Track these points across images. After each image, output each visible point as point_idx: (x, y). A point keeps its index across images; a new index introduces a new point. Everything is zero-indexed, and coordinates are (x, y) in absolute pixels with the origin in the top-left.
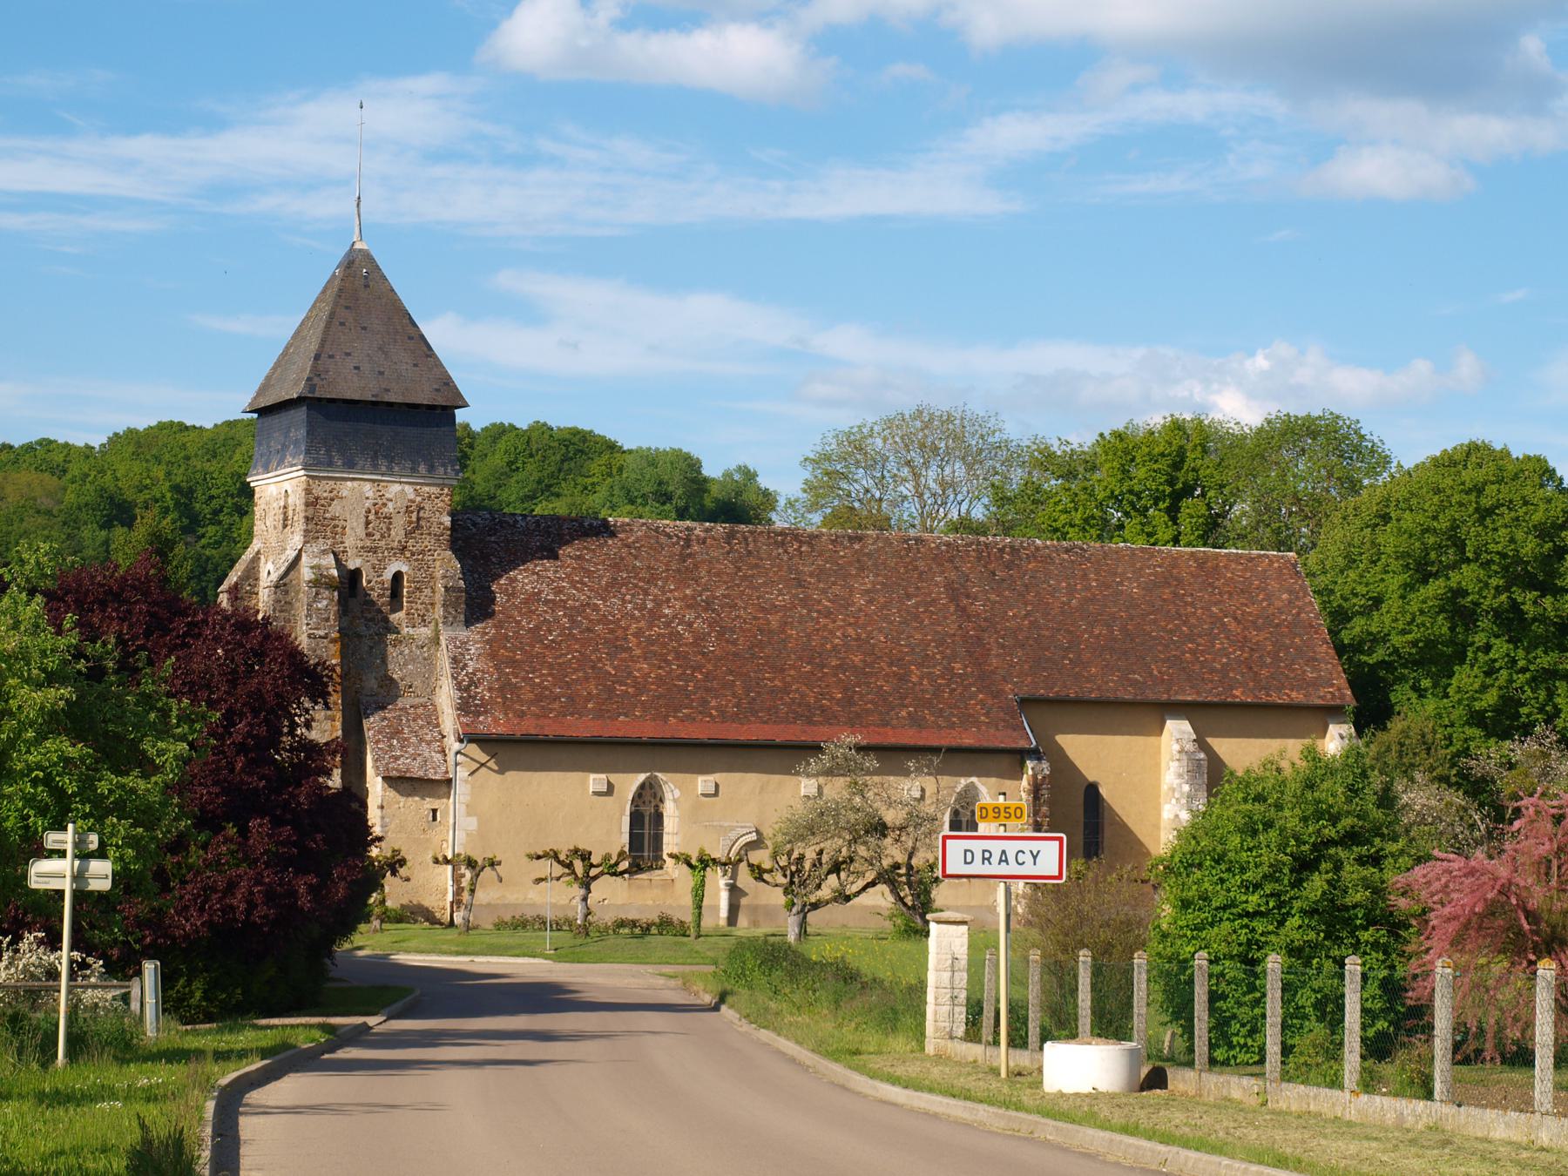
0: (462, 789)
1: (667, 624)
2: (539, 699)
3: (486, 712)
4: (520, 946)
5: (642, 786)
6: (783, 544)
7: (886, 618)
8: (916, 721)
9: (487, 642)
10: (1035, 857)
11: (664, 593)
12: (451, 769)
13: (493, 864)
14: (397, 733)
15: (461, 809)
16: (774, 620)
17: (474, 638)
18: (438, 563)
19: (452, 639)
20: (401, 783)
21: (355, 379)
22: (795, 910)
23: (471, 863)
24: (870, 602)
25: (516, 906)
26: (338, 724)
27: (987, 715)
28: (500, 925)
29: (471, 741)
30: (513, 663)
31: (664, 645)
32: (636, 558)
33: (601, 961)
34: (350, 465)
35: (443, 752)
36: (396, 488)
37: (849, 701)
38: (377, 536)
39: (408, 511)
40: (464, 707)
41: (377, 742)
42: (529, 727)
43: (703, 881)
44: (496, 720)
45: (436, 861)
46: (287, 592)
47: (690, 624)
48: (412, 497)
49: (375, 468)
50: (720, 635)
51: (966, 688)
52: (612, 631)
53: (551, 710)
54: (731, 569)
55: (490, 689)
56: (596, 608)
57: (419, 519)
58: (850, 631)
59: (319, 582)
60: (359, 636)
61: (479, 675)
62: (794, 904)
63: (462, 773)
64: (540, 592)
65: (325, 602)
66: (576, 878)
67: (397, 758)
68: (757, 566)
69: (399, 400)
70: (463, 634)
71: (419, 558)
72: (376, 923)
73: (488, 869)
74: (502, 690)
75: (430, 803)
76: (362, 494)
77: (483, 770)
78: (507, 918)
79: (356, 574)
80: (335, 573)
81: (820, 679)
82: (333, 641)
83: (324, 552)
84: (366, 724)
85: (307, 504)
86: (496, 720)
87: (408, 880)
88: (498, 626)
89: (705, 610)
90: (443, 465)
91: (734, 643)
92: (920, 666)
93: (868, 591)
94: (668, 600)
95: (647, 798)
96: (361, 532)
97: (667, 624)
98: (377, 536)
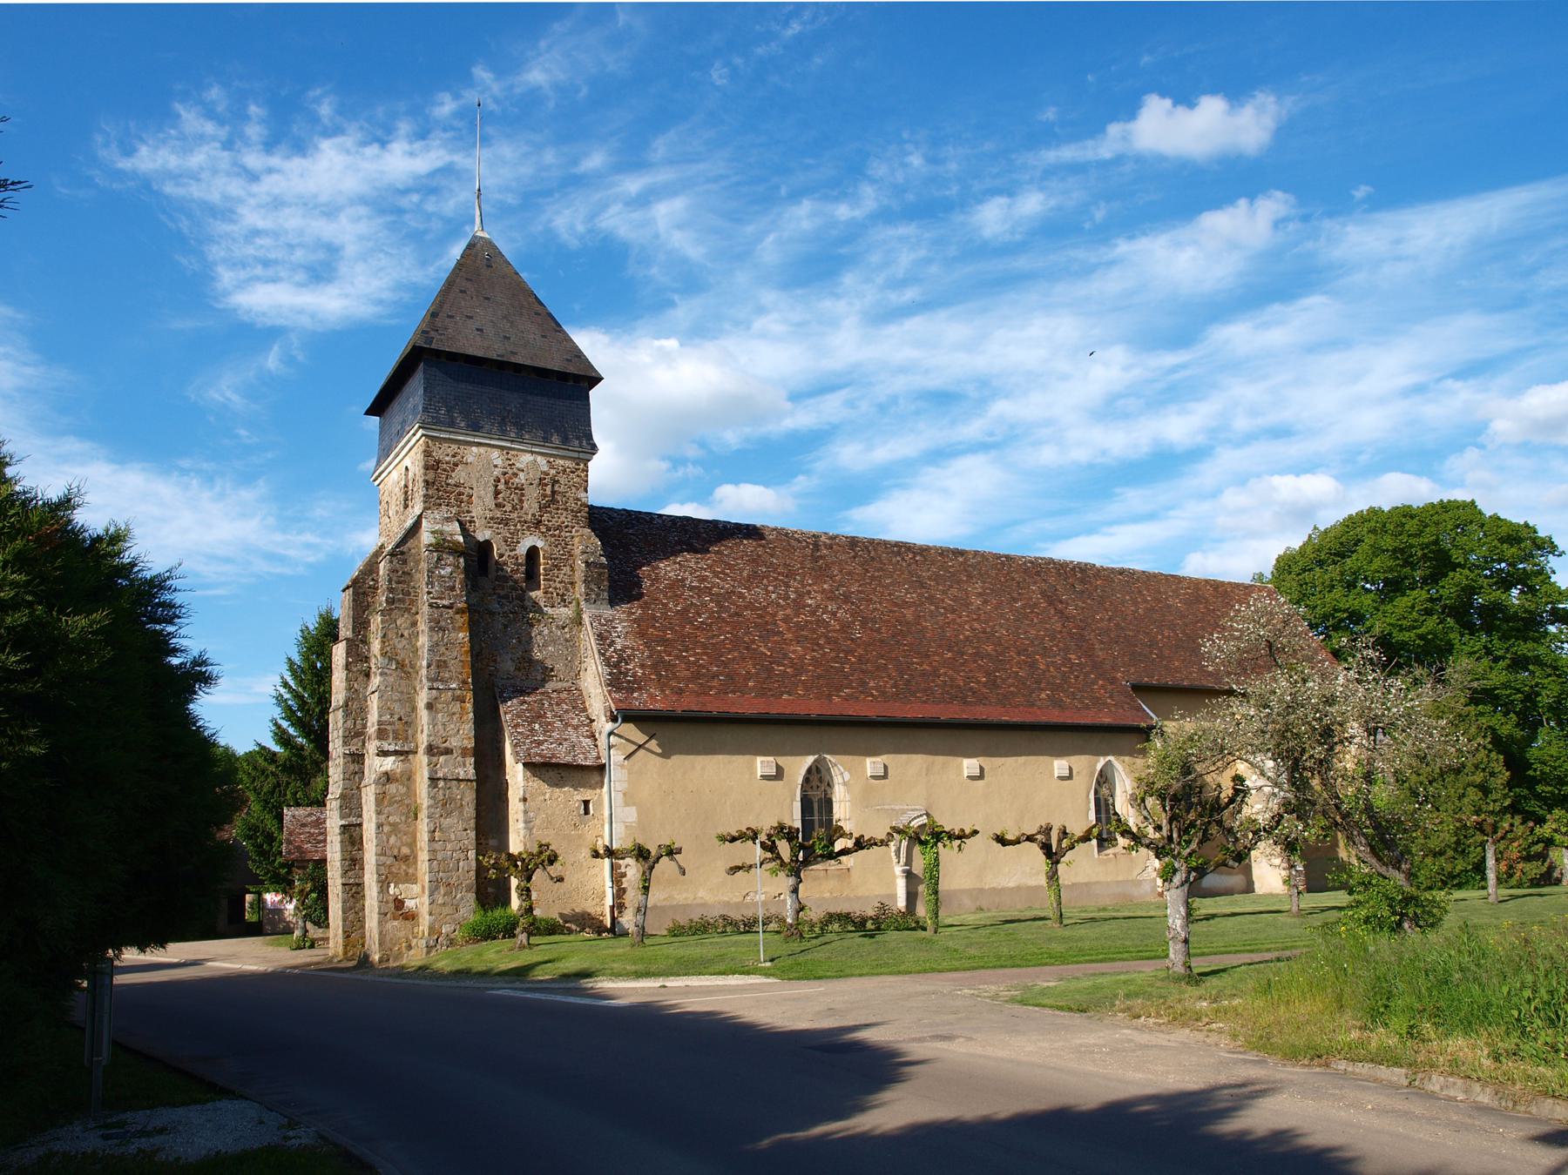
0: (617, 775)
1: (813, 613)
2: (696, 677)
3: (640, 689)
4: (722, 957)
5: (809, 771)
6: (899, 553)
7: (1002, 616)
8: (1058, 704)
9: (635, 621)
11: (804, 586)
12: (604, 754)
13: (671, 852)
14: (539, 717)
15: (618, 798)
16: (909, 614)
17: (621, 618)
18: (576, 540)
19: (597, 618)
20: (544, 769)
21: (478, 339)
22: (1177, 879)
23: (641, 854)
24: (985, 602)
25: (685, 907)
26: (469, 706)
27: (1111, 697)
28: (677, 931)
29: (626, 719)
30: (663, 641)
31: (814, 631)
33: (841, 975)
34: (475, 427)
35: (593, 736)
36: (528, 458)
37: (993, 684)
38: (508, 508)
39: (541, 482)
40: (616, 682)
41: (517, 726)
42: (689, 703)
43: (937, 859)
44: (652, 697)
45: (596, 855)
46: (405, 562)
47: (834, 614)
48: (545, 469)
49: (503, 434)
50: (864, 624)
51: (1087, 675)
52: (760, 616)
53: (711, 688)
54: (859, 570)
55: (642, 666)
56: (741, 596)
57: (553, 492)
58: (976, 625)
59: (441, 547)
60: (492, 613)
61: (629, 652)
62: (1175, 871)
63: (617, 757)
64: (683, 580)
65: (449, 569)
66: (783, 864)
67: (540, 743)
68: (881, 569)
69: (528, 362)
70: (608, 612)
71: (555, 534)
72: (523, 937)
73: (665, 859)
74: (655, 666)
75: (580, 795)
76: (489, 462)
77: (642, 751)
78: (683, 921)
79: (486, 546)
80: (461, 539)
81: (962, 664)
82: (460, 611)
83: (448, 519)
84: (502, 709)
85: (427, 467)
86: (652, 697)
87: (561, 879)
88: (645, 607)
89: (845, 602)
90: (578, 438)
91: (878, 631)
92: (1043, 656)
93: (980, 594)
94: (809, 592)
95: (815, 783)
96: (490, 501)
97: (813, 613)
98: (508, 508)
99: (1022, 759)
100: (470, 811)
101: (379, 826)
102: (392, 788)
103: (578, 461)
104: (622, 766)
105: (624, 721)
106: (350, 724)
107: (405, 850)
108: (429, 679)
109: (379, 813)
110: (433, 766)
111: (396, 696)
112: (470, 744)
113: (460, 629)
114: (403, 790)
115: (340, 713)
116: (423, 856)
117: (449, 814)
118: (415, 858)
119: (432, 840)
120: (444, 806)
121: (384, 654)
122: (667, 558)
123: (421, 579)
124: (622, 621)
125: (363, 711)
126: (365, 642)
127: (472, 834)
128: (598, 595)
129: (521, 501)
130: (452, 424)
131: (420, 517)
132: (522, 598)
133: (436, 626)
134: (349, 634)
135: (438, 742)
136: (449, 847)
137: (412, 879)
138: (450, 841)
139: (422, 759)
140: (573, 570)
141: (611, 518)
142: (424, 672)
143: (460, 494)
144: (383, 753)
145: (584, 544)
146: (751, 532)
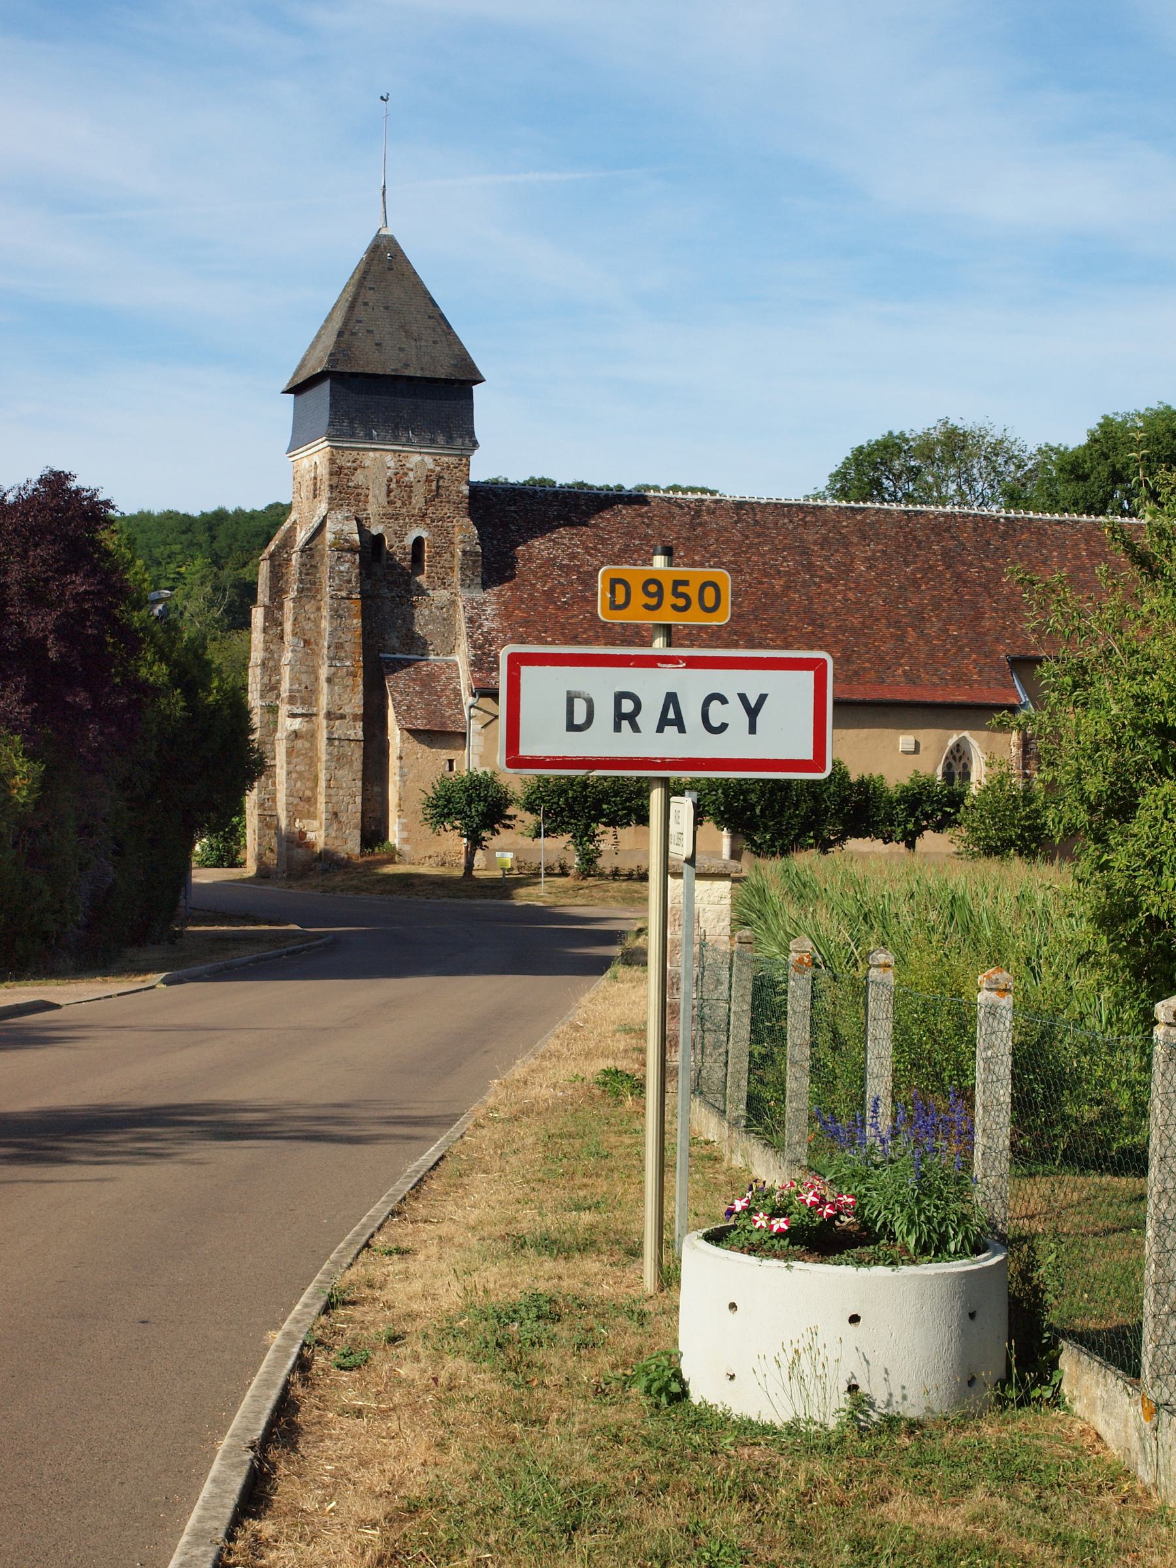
10: (753, 712)
17: (491, 599)
18: (456, 529)
26: (360, 680)
32: (648, 526)
34: (369, 437)
36: (416, 458)
38: (399, 504)
39: (428, 480)
46: (312, 557)
48: (431, 466)
49: (395, 439)
54: (738, 537)
57: (438, 487)
59: (342, 547)
61: (494, 633)
64: (555, 558)
65: (347, 565)
70: (479, 595)
71: (440, 527)
76: (383, 463)
79: (379, 538)
80: (357, 537)
83: (347, 518)
85: (331, 474)
96: (383, 500)
98: (399, 504)
99: (865, 732)
100: (358, 765)
101: (289, 773)
102: (299, 743)
103: (460, 457)
104: (480, 734)
105: (481, 696)
106: (266, 679)
107: (308, 793)
108: (329, 658)
109: (289, 763)
110: (330, 729)
111: (304, 668)
112: (360, 711)
113: (355, 617)
114: (307, 745)
115: (258, 671)
116: (322, 799)
117: (342, 767)
118: (316, 799)
119: (328, 787)
120: (338, 760)
121: (295, 634)
122: (543, 534)
123: (324, 572)
124: (493, 604)
125: (276, 670)
126: (281, 607)
127: (359, 784)
128: (472, 580)
129: (410, 497)
130: (353, 435)
131: (325, 517)
132: (408, 583)
133: (336, 614)
134: (267, 601)
135: (335, 709)
136: (341, 792)
137: (312, 816)
138: (342, 788)
139: (322, 722)
140: (453, 556)
141: (496, 495)
142: (325, 651)
143: (358, 495)
144: (293, 716)
145: (464, 533)
146: (637, 499)
